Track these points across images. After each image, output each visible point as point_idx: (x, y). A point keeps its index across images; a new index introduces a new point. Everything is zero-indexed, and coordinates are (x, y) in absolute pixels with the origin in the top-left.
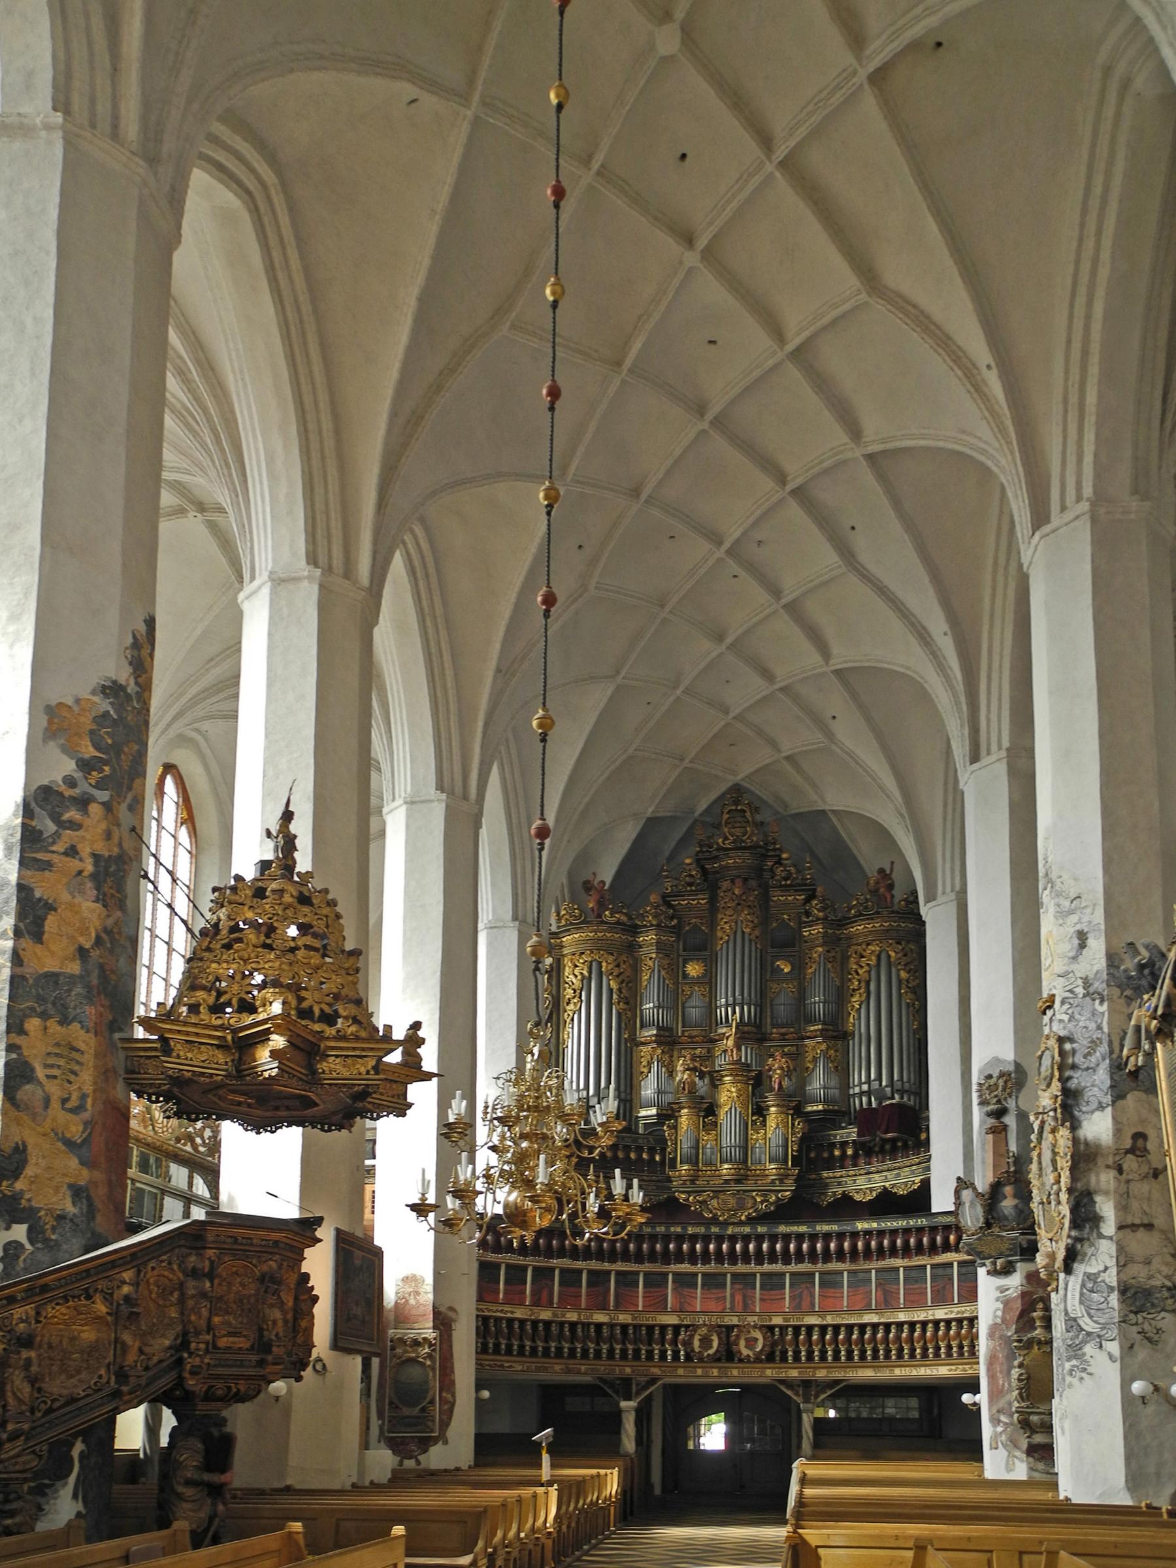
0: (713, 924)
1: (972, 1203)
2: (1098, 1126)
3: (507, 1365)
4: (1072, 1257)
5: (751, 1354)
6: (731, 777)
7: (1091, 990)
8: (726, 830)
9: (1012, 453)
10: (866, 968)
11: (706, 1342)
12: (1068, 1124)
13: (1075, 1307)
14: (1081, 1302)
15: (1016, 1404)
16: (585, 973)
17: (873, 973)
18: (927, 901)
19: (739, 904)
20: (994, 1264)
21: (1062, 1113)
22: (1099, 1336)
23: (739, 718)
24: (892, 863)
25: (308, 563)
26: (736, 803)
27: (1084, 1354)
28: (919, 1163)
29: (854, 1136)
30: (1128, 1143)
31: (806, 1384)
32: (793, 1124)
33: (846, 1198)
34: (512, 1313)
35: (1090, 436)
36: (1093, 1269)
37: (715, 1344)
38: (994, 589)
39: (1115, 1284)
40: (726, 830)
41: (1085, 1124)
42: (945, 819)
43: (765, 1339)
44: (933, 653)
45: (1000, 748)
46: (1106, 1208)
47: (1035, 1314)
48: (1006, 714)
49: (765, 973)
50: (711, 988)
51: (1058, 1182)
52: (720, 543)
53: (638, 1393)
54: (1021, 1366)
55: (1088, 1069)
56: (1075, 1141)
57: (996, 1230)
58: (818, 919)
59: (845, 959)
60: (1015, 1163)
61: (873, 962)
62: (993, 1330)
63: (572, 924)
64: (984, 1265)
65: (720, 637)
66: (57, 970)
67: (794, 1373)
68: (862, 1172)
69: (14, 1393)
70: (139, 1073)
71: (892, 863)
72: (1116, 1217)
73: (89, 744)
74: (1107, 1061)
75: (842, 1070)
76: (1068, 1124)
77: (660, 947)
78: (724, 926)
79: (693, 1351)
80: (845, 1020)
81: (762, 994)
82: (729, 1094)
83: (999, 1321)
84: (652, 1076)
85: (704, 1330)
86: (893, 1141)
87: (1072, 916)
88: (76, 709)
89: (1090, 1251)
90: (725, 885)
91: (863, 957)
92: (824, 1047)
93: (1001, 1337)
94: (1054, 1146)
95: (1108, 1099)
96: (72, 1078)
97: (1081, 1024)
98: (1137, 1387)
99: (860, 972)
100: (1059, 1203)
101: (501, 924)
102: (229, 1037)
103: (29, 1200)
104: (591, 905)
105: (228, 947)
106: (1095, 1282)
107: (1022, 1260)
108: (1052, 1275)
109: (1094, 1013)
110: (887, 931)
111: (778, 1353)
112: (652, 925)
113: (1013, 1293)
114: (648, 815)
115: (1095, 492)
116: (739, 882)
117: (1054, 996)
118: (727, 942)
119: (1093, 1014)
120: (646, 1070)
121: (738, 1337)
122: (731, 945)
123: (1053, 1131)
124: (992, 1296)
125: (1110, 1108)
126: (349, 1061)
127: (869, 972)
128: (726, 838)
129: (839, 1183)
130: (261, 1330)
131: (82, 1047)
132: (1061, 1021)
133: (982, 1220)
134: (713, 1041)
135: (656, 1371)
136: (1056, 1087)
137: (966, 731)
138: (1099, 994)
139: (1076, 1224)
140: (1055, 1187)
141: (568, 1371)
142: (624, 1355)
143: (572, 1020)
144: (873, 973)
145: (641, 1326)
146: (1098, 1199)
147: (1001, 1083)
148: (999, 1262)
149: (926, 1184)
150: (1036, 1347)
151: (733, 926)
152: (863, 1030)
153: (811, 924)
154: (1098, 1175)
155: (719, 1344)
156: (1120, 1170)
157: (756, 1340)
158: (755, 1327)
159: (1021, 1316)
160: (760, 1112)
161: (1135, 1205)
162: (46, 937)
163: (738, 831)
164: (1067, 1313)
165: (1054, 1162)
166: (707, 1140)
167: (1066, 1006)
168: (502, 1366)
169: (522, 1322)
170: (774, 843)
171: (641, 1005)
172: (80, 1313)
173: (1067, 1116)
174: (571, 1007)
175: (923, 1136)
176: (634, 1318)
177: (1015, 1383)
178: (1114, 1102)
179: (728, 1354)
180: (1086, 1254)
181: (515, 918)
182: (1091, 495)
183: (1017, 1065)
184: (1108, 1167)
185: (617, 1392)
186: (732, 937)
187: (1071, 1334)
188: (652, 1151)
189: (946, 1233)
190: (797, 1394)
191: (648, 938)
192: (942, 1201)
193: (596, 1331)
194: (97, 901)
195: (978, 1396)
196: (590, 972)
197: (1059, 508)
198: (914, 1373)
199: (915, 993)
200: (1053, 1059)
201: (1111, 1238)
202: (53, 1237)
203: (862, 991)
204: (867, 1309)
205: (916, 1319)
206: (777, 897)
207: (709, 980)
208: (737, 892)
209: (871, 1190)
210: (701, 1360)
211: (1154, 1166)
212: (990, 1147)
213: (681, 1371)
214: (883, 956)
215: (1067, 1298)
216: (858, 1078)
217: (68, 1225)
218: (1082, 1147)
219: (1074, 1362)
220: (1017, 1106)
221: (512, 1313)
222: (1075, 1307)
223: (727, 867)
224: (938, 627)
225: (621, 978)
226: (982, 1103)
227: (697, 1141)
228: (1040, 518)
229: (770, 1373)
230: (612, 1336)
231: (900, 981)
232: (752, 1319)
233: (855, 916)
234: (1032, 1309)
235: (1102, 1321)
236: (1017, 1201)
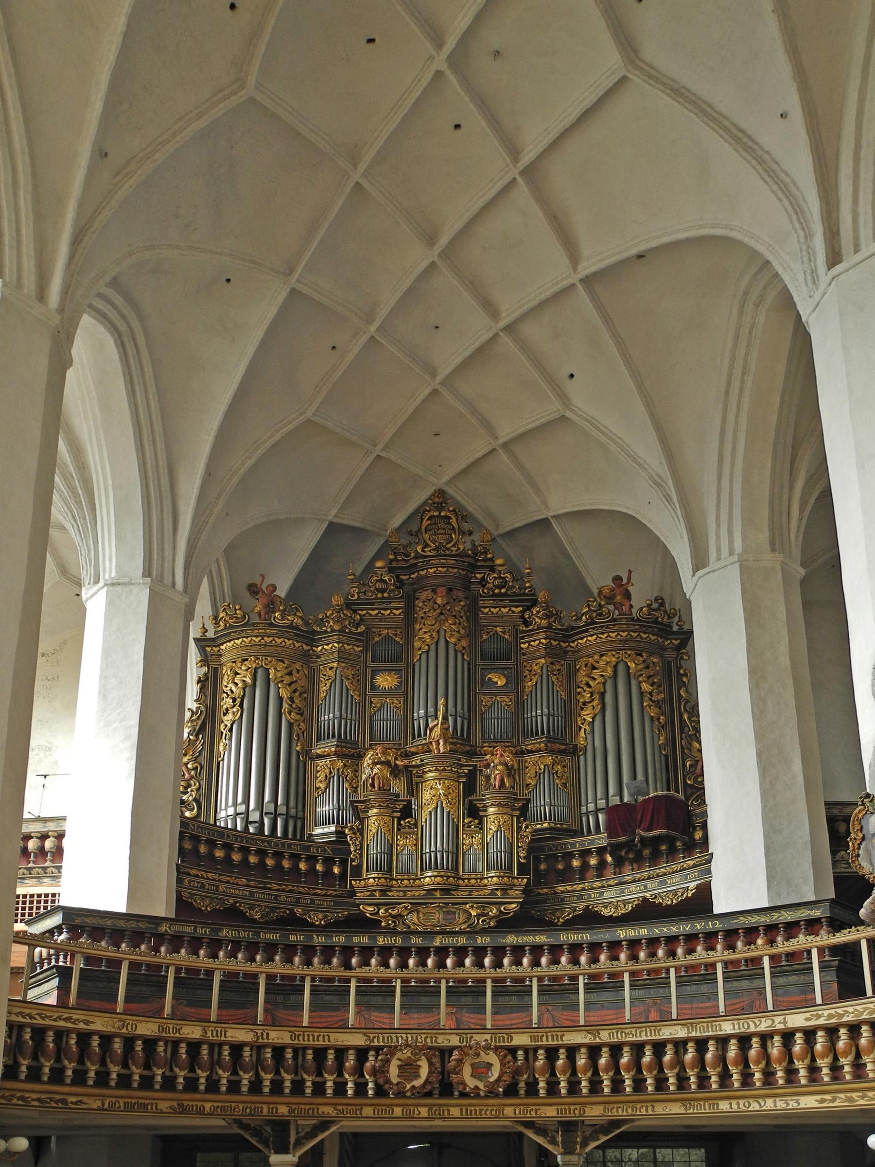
3: (74, 1099)
6: (433, 479)
10: (599, 679)
11: (409, 1069)
16: (248, 680)
17: (609, 686)
19: (441, 614)
26: (440, 507)
28: (695, 866)
31: (568, 1127)
32: (519, 828)
34: (87, 1022)
37: (424, 1072)
43: (503, 1064)
44: (761, 161)
49: (474, 684)
53: (299, 1143)
59: (572, 673)
63: (231, 627)
67: (551, 1112)
77: (343, 657)
78: (423, 636)
79: (388, 1081)
81: (471, 707)
82: (433, 791)
85: (407, 1053)
91: (594, 668)
92: (549, 760)
101: (126, 580)
110: (625, 641)
112: (333, 631)
114: (331, 517)
116: (442, 591)
118: (428, 652)
120: (322, 786)
121: (460, 1061)
122: (432, 654)
127: (604, 684)
129: (580, 897)
135: (328, 1110)
141: (183, 1110)
142: (277, 1087)
143: (231, 730)
144: (609, 686)
145: (305, 1049)
151: (435, 636)
152: (598, 743)
153: (531, 633)
155: (430, 1072)
157: (489, 1065)
158: (487, 1048)
160: (475, 813)
163: (441, 539)
166: (405, 845)
168: (64, 1102)
169: (106, 1039)
170: (485, 553)
174: (230, 717)
175: (698, 835)
176: (294, 1036)
179: (445, 1086)
181: (147, 572)
185: (266, 1143)
186: (433, 648)
190: (553, 1142)
191: (328, 648)
196: (254, 679)
199: (660, 708)
204: (665, 1019)
205: (753, 1029)
206: (489, 610)
207: (405, 692)
209: (625, 903)
210: (401, 1094)
213: (368, 1111)
214: (621, 667)
223: (426, 577)
225: (293, 686)
227: (391, 847)
229: (512, 1111)
230: (259, 1061)
231: (642, 694)
232: (481, 1038)
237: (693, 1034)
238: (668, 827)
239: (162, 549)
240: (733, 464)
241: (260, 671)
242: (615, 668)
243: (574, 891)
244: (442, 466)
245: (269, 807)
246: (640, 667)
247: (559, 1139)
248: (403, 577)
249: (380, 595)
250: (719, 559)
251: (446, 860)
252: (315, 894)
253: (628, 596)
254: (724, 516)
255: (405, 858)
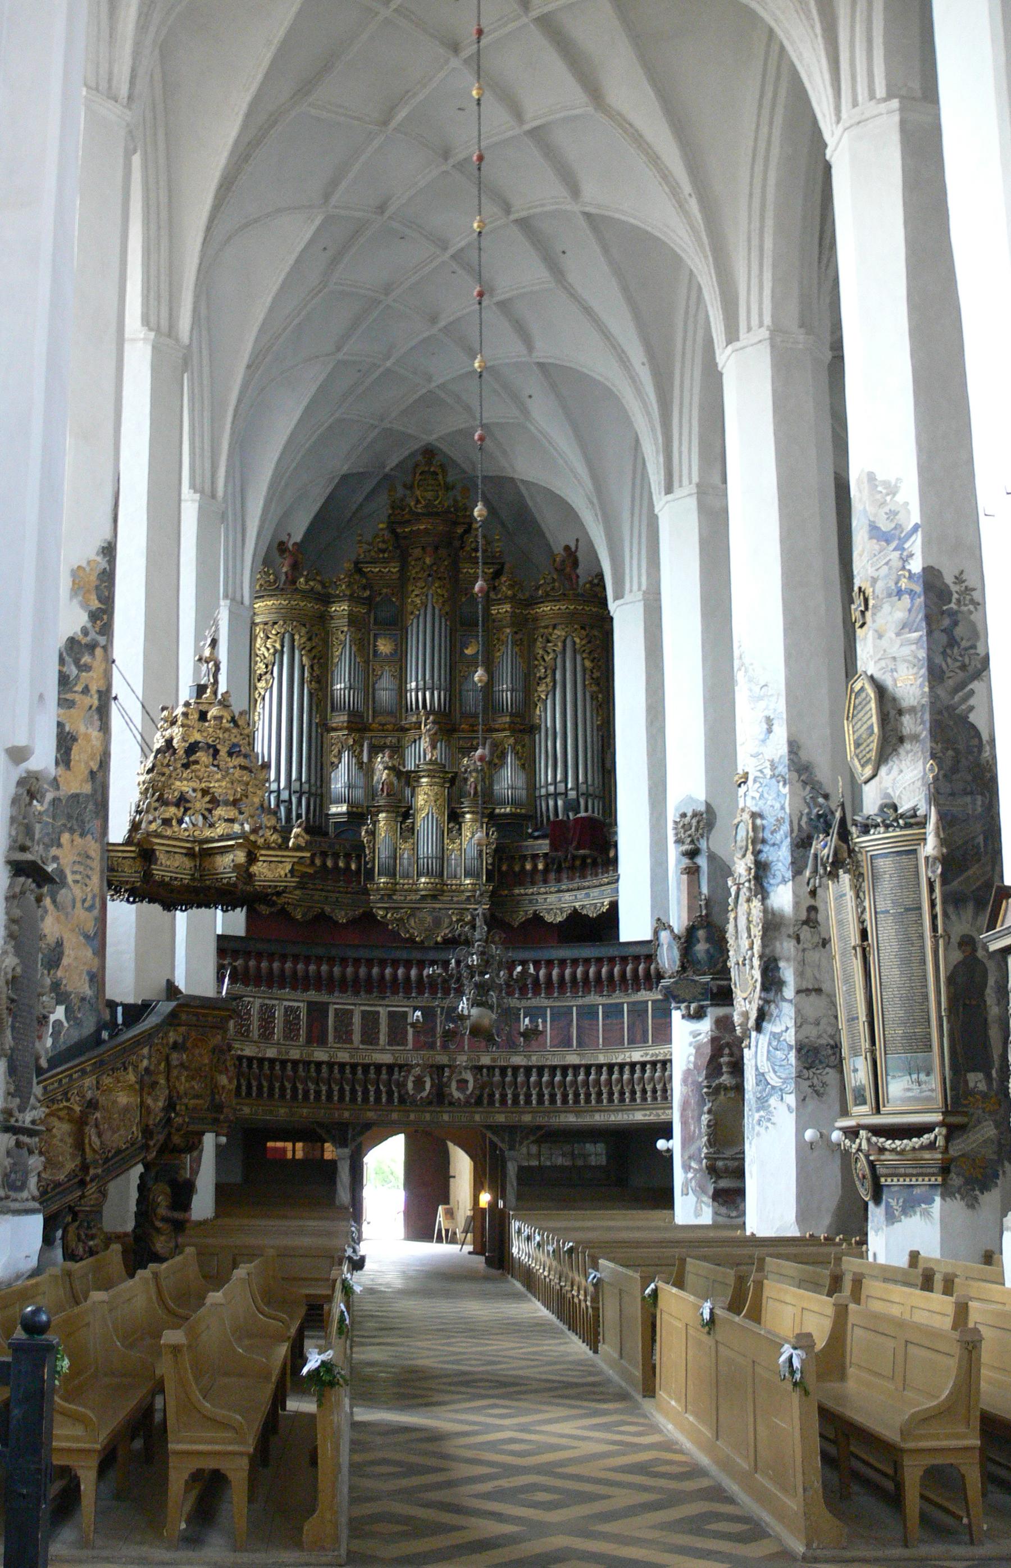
0: (403, 595)
1: (670, 947)
2: (783, 897)
4: (762, 1016)
5: (462, 1097)
7: (777, 773)
8: (418, 493)
9: (708, 266)
11: (419, 1083)
12: (759, 896)
13: (765, 1066)
14: (768, 1059)
15: (705, 1150)
16: (278, 646)
17: (559, 661)
18: (616, 598)
19: (429, 575)
20: (688, 1008)
21: (755, 885)
22: (781, 1090)
23: (442, 387)
24: (577, 540)
25: (143, 325)
27: (769, 1106)
29: (546, 850)
30: (804, 916)
33: (537, 919)
35: (768, 276)
36: (777, 1029)
37: (428, 1086)
38: (685, 332)
39: (793, 1043)
40: (418, 493)
41: (772, 895)
42: (632, 514)
44: (634, 381)
45: (690, 483)
46: (788, 973)
47: (722, 1060)
48: (695, 450)
50: (401, 669)
51: (751, 948)
52: (445, 249)
54: (709, 1112)
55: (774, 845)
56: (765, 911)
57: (690, 973)
58: (506, 597)
60: (707, 905)
61: (559, 648)
62: (688, 1073)
64: (679, 1008)
65: (434, 319)
66: (78, 791)
68: (553, 889)
69: (90, 1145)
70: (117, 871)
71: (577, 540)
72: (796, 983)
73: (95, 597)
74: (789, 839)
75: (528, 765)
76: (759, 896)
77: (353, 621)
79: (407, 1093)
80: (531, 715)
82: (425, 798)
83: (691, 1066)
84: (343, 767)
85: (417, 1071)
86: (584, 858)
87: (761, 702)
88: (88, 569)
89: (775, 1012)
90: (417, 552)
91: (548, 641)
93: (692, 1083)
94: (749, 914)
95: (789, 874)
96: (87, 881)
97: (769, 803)
98: (809, 1134)
99: (547, 658)
100: (752, 967)
102: (197, 849)
103: (65, 986)
104: (284, 569)
105: (186, 766)
106: (779, 1041)
107: (712, 1005)
108: (746, 1034)
109: (778, 794)
111: (485, 1095)
113: (705, 1038)
115: (773, 322)
117: (747, 773)
119: (778, 795)
121: (450, 1078)
123: (749, 900)
124: (687, 1039)
125: (790, 883)
126: (273, 865)
127: (555, 659)
128: (418, 502)
130: (213, 1093)
131: (92, 854)
132: (753, 798)
133: (678, 963)
134: (404, 730)
135: (371, 1115)
136: (750, 858)
137: (661, 460)
138: (783, 777)
139: (765, 988)
140: (749, 953)
143: (264, 699)
144: (559, 661)
146: (782, 964)
147: (694, 822)
148: (693, 1006)
149: (614, 906)
150: (723, 1093)
152: (549, 724)
153: (500, 602)
154: (781, 944)
155: (432, 1086)
156: (798, 940)
157: (467, 1081)
158: (466, 1068)
159: (710, 1062)
160: (455, 817)
161: (809, 972)
162: (72, 763)
164: (757, 1069)
165: (749, 930)
167: (757, 785)
171: (332, 686)
172: (119, 1082)
173: (758, 887)
175: (612, 854)
176: (352, 1057)
177: (704, 1129)
178: (794, 877)
180: (772, 1015)
182: (770, 324)
183: (708, 806)
184: (789, 936)
186: (422, 611)
187: (760, 1088)
188: (348, 857)
189: (638, 965)
190: (503, 1141)
191: (340, 609)
192: (634, 926)
193: (293, 1068)
194: (100, 730)
195: (671, 1141)
196: (282, 646)
197: (746, 330)
198: (613, 1118)
199: (598, 684)
200: (748, 833)
201: (791, 1001)
202: (79, 1016)
203: (548, 680)
205: (614, 1061)
207: (399, 660)
208: (428, 561)
210: (414, 1102)
211: (823, 936)
212: (684, 887)
215: (757, 1056)
216: (545, 775)
217: (88, 1006)
218: (770, 916)
219: (762, 1113)
220: (708, 848)
221: (242, 1050)
222: (765, 1066)
224: (637, 355)
226: (679, 841)
228: (732, 336)
231: (584, 669)
233: (542, 597)
234: (724, 1059)
235: (783, 1076)
236: (707, 946)
237: (583, 1062)
238: (590, 849)
239: (235, 562)
240: (641, 505)
241: (287, 635)
242: (564, 642)
243: (526, 894)
244: (437, 430)
245: (295, 786)
246: (584, 642)
247: (507, 1139)
248: (398, 530)
249: (381, 556)
250: (631, 591)
251: (435, 865)
252: (339, 892)
253: (575, 563)
254: (635, 551)
255: (405, 862)
